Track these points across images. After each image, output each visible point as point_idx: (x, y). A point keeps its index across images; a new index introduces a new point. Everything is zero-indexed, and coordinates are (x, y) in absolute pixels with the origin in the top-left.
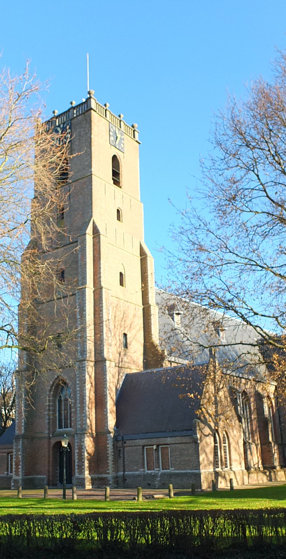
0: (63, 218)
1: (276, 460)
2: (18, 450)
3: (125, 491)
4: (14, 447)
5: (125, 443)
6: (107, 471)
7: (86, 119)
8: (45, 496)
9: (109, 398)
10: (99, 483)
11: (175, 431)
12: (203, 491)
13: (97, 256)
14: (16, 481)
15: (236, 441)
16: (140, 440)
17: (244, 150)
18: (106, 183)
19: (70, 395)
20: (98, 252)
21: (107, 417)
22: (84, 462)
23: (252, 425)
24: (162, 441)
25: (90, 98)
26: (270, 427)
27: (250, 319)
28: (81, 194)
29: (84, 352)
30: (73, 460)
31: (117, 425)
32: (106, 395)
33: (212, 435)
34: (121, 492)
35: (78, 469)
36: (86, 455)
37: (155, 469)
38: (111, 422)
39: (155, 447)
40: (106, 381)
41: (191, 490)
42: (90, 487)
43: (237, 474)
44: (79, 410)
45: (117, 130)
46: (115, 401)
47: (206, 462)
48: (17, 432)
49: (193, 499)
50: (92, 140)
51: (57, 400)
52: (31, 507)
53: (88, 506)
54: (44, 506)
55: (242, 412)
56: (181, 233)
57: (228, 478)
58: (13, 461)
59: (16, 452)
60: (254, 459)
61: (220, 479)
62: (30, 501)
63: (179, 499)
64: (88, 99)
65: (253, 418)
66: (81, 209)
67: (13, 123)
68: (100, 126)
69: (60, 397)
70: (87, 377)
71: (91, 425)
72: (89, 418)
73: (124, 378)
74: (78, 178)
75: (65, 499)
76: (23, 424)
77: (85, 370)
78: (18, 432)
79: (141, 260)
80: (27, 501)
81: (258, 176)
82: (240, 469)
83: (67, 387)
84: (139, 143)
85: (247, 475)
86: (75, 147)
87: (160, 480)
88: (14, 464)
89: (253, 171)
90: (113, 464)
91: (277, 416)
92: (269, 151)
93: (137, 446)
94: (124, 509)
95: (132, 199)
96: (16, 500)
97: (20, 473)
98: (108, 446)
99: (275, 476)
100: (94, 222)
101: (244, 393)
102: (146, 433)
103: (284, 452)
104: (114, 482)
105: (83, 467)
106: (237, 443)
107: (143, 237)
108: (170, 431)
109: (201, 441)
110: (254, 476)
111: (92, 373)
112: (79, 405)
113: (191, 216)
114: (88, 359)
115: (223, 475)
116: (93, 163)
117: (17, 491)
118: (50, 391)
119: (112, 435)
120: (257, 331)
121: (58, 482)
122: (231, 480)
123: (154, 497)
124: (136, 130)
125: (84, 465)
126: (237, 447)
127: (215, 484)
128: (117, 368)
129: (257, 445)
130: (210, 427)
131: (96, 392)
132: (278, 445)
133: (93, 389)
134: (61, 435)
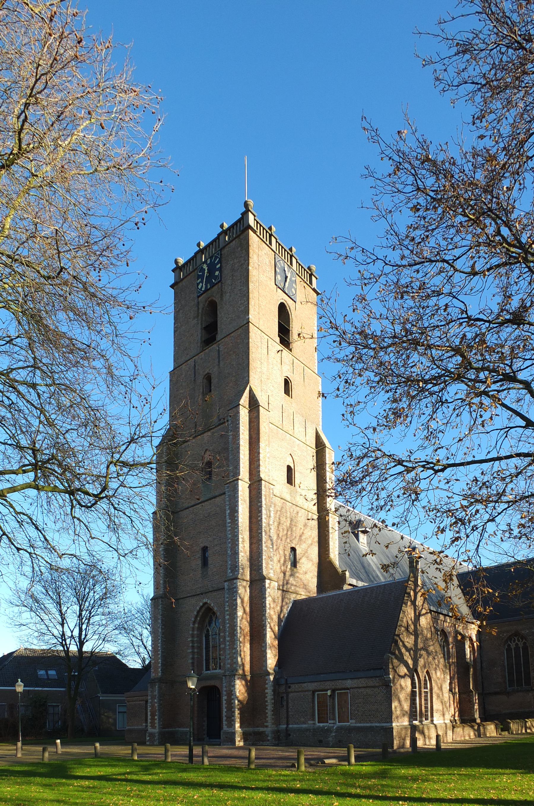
0: (210, 391)
2: (153, 697)
4: (149, 693)
5: (290, 687)
6: (265, 724)
14: (152, 735)
16: (309, 684)
22: (234, 712)
24: (339, 684)
25: (247, 211)
26: (471, 673)
28: (234, 352)
29: (235, 567)
31: (279, 664)
35: (226, 720)
36: (236, 701)
37: (329, 722)
38: (271, 660)
39: (329, 693)
40: (265, 606)
41: (379, 750)
42: (242, 744)
45: (286, 267)
47: (398, 712)
48: (153, 675)
50: (250, 274)
64: (245, 214)
68: (261, 258)
71: (243, 665)
72: (240, 655)
75: (192, 763)
76: (160, 665)
79: (317, 452)
82: (442, 722)
87: (335, 736)
88: (149, 713)
90: (273, 715)
91: (479, 660)
93: (305, 691)
95: (305, 367)
97: (157, 725)
98: (266, 691)
100: (251, 390)
103: (484, 703)
106: (441, 689)
107: (321, 423)
114: (239, 576)
118: (194, 623)
119: (272, 678)
121: (205, 736)
123: (324, 763)
124: (314, 273)
125: (234, 716)
126: (441, 693)
128: (280, 592)
130: (407, 665)
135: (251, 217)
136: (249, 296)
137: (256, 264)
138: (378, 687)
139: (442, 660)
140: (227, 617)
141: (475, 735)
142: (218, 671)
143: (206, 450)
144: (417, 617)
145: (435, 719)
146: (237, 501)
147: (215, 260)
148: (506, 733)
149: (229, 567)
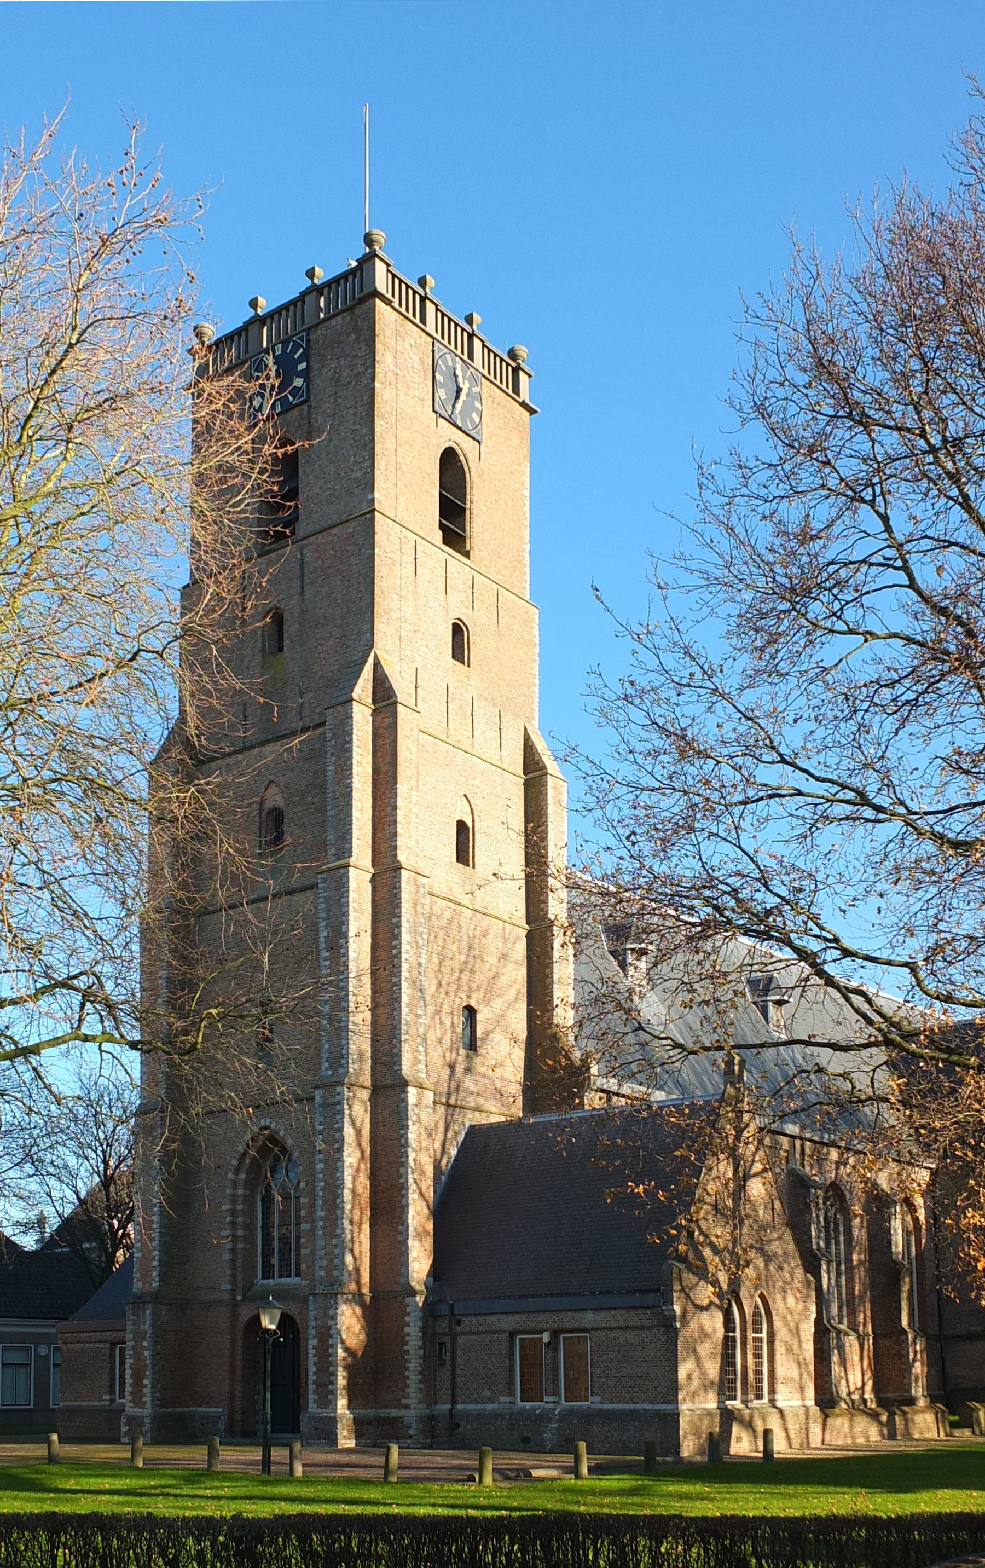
0: (281, 649)
1: (916, 1381)
2: (139, 1336)
3: (453, 1457)
4: (130, 1326)
5: (459, 1323)
6: (403, 1401)
7: (356, 329)
8: (210, 1465)
9: (413, 1196)
10: (374, 1432)
11: (609, 1293)
12: (680, 1460)
13: (385, 768)
14: (134, 1422)
15: (792, 1324)
16: (502, 1316)
17: (841, 433)
18: (419, 540)
19: (299, 1183)
20: (388, 759)
21: (407, 1248)
22: (334, 1374)
23: (850, 1280)
24: (568, 1319)
25: (372, 256)
26: (906, 1288)
27: (830, 969)
28: (338, 571)
29: (339, 1057)
30: (303, 1367)
31: (436, 1271)
32: (404, 1187)
33: (720, 1307)
34: (439, 1458)
36: (341, 1353)
38: (419, 1262)
39: (546, 1337)
40: (406, 1145)
42: (351, 1444)
43: (789, 1417)
44: (323, 1228)
46: (431, 1204)
48: (137, 1286)
49: (646, 1482)
50: (377, 399)
51: (259, 1199)
52: (163, 1494)
53: (329, 1495)
54: (201, 1492)
55: (822, 1244)
56: (626, 698)
57: (760, 1429)
58: (127, 1366)
59: (133, 1339)
60: (851, 1378)
61: (736, 1429)
62: (163, 1476)
63: (603, 1483)
64: (367, 260)
65: (855, 1263)
66: (339, 622)
67: (84, 331)
68: (402, 353)
69: (268, 1188)
70: (348, 1131)
71: (357, 1270)
72: (352, 1251)
73: (461, 1137)
74: (330, 522)
75: (269, 1473)
76: (155, 1263)
77: (341, 1112)
78: (141, 1284)
79: (527, 784)
80: (154, 1477)
81: (885, 519)
82: (799, 1403)
83: (289, 1159)
84: (532, 412)
85: (820, 1420)
86: (320, 420)
87: (558, 1429)
88: (128, 1373)
89: (872, 503)
92: (923, 435)
93: (495, 1332)
94: (433, 1505)
96: (124, 1472)
97: (147, 1399)
98: (406, 1330)
99: (906, 1425)
100: (377, 665)
101: (836, 1190)
102: (520, 1297)
103: (943, 1359)
104: (423, 1432)
105: (330, 1387)
106: (797, 1333)
107: (536, 715)
108: (593, 1293)
109: (685, 1322)
110: (840, 1423)
111: (363, 1121)
112: (320, 1214)
113: (663, 643)
115: (747, 1418)
116: (377, 472)
117: (130, 1447)
118: (237, 1170)
119: (420, 1300)
120: (851, 1004)
122: (767, 1433)
123: (531, 1475)
124: (523, 365)
125: (334, 1382)
126: (796, 1342)
127: (717, 1444)
128: (441, 1109)
129: (861, 1339)
131: (374, 1176)
132: (928, 1338)
133: (366, 1166)
134: (261, 1300)
135: (380, 267)
136: (373, 448)
137: (390, 375)
138: (649, 1328)
139: (799, 1273)
140: (320, 1166)
141: (882, 1435)
142: (293, 1280)
143: (271, 782)
144: (742, 1180)
145: (778, 1397)
146: (346, 914)
147: (294, 350)
148: (967, 1432)
149: (326, 1055)
